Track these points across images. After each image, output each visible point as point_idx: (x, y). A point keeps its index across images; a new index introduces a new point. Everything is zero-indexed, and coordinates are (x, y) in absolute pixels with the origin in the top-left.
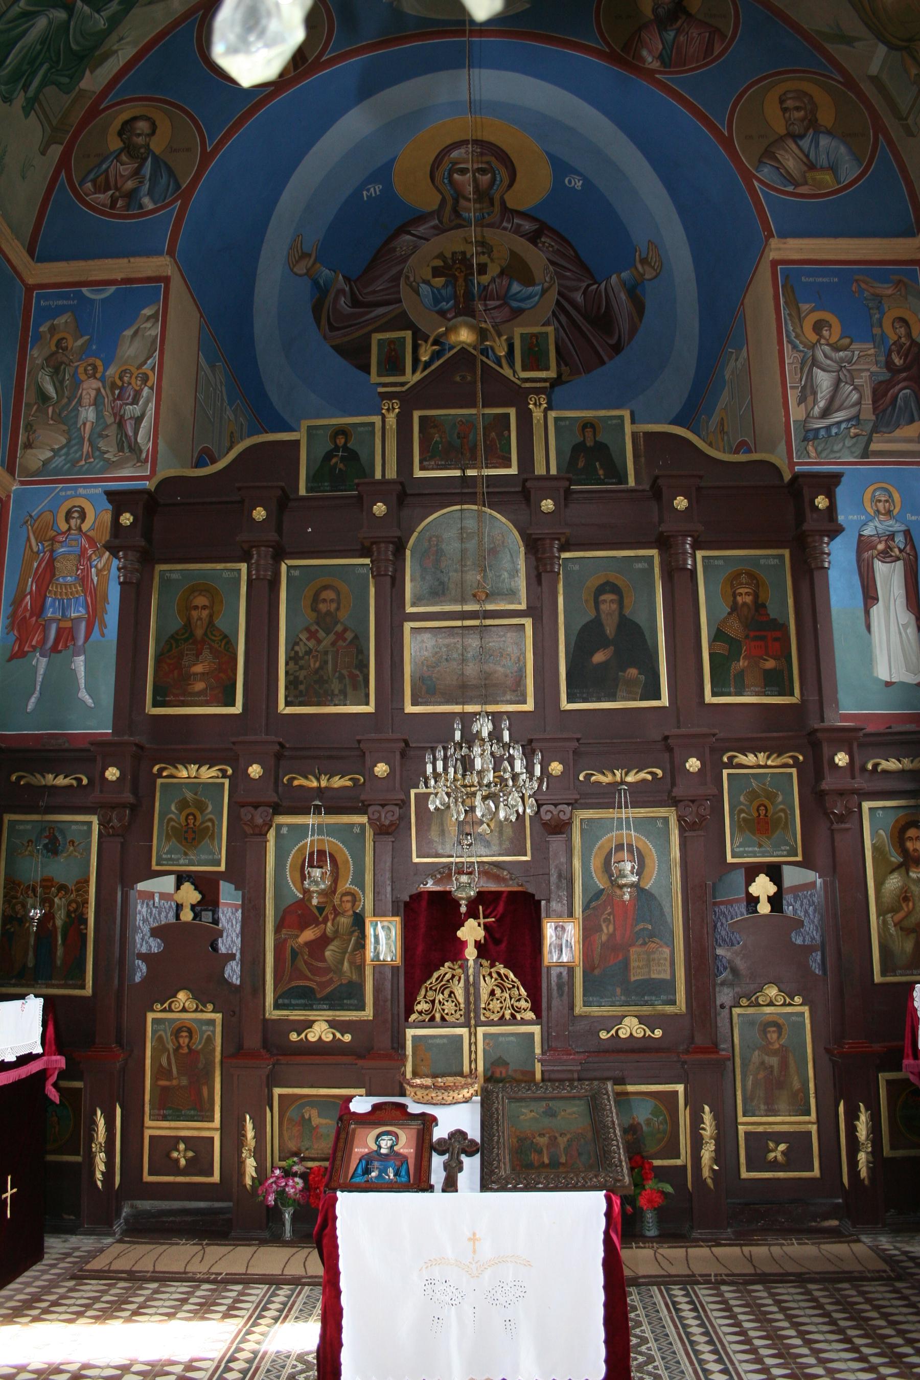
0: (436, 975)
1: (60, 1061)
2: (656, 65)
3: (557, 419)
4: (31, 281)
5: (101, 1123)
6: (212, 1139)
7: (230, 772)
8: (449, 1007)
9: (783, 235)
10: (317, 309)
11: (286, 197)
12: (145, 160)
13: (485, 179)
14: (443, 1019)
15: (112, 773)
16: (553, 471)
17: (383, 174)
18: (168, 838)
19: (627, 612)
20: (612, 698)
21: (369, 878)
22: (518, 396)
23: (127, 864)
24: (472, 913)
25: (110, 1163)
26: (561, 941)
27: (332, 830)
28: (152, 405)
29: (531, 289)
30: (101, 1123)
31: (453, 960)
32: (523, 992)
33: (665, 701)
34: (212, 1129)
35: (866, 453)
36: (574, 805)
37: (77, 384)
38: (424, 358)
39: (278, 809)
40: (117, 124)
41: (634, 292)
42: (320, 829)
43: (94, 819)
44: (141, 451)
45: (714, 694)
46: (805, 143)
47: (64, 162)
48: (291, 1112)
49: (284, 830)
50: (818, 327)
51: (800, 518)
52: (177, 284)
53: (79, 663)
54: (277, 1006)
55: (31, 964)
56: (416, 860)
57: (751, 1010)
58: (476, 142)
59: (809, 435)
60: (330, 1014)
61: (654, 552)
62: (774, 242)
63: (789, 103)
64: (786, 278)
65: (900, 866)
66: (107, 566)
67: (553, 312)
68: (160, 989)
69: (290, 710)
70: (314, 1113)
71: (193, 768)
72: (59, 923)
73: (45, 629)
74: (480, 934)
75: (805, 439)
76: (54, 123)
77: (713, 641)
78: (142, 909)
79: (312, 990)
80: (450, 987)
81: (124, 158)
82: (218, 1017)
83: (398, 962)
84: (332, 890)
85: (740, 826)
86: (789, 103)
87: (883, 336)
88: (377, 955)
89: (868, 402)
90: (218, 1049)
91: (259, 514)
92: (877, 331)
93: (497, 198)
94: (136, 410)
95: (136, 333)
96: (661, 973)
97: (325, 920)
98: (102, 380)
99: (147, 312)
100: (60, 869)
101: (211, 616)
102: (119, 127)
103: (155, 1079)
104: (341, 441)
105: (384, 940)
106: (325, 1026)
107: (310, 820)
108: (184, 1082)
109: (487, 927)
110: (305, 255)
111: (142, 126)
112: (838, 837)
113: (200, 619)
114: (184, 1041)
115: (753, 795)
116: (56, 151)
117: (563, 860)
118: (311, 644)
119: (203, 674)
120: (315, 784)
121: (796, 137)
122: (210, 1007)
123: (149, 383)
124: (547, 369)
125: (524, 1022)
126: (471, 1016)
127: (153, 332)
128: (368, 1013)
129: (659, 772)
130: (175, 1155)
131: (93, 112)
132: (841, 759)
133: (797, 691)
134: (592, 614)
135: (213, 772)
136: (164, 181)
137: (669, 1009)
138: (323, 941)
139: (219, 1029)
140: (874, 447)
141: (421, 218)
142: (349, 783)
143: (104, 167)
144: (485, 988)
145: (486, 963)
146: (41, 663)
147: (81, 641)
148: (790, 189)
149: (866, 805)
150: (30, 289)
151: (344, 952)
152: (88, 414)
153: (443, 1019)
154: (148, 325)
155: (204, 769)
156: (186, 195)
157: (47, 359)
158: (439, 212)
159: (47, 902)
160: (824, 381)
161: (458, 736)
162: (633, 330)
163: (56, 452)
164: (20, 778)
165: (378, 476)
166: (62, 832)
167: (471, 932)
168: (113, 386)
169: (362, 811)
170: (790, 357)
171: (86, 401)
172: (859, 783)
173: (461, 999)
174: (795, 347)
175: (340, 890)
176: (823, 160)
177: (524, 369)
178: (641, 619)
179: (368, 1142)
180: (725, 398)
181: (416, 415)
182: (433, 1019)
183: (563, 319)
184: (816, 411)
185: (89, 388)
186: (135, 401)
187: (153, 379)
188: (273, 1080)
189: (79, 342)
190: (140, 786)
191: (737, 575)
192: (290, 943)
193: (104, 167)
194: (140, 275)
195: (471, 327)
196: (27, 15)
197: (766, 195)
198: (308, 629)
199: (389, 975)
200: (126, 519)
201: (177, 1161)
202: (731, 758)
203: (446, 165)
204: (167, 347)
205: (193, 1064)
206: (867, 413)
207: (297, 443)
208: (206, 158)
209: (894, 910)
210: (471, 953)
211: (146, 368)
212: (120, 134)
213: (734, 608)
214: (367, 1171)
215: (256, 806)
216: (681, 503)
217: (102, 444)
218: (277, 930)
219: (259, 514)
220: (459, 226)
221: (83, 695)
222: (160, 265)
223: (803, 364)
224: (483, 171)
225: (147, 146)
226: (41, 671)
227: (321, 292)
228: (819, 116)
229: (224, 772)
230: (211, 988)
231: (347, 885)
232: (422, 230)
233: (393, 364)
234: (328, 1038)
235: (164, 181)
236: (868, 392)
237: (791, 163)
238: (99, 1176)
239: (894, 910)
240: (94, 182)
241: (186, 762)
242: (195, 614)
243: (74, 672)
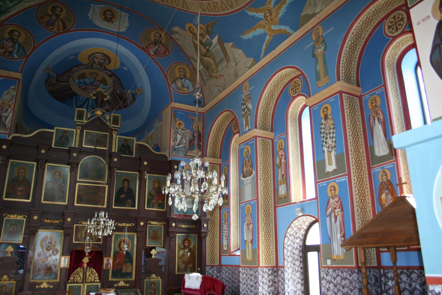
0: (76, 270)
2: (153, 54)
3: (119, 138)
7: (26, 217)
8: (79, 278)
9: (175, 102)
10: (46, 81)
11: (50, 56)
12: (16, 43)
13: (102, 61)
14: (77, 281)
16: (116, 151)
17: (76, 55)
19: (130, 186)
20: (124, 206)
22: (111, 131)
26: (108, 262)
28: (11, 114)
32: (97, 275)
33: (136, 208)
35: (186, 155)
41: (134, 97)
44: (6, 126)
45: (147, 207)
46: (183, 80)
50: (180, 124)
51: (200, 229)
57: (149, 280)
58: (102, 53)
59: (174, 149)
61: (137, 173)
62: (173, 103)
63: (181, 70)
64: (174, 111)
65: (183, 248)
69: (44, 202)
75: (173, 150)
77: (148, 195)
81: (9, 41)
85: (150, 238)
86: (181, 70)
87: (193, 129)
89: (188, 143)
92: (192, 127)
93: (104, 66)
95: (8, 92)
96: (129, 271)
99: (12, 87)
102: (9, 31)
104: (65, 134)
109: (89, 259)
110: (49, 69)
111: (16, 33)
112: (171, 242)
113: (21, 175)
115: (154, 231)
119: (21, 190)
121: (181, 79)
122: (159, 277)
123: (11, 108)
125: (97, 282)
129: (133, 224)
132: (174, 225)
133: (165, 208)
134: (122, 186)
135: (22, 217)
136: (21, 51)
137: (131, 279)
140: (188, 154)
141: (82, 65)
142: (59, 222)
143: (3, 42)
144: (88, 274)
145: (89, 268)
148: (178, 91)
149: (177, 235)
153: (77, 281)
154: (12, 91)
156: (27, 57)
158: (87, 65)
160: (179, 137)
161: (96, 216)
162: (131, 104)
167: (86, 260)
170: (173, 130)
172: (176, 230)
174: (174, 128)
176: (186, 85)
177: (113, 124)
178: (133, 188)
180: (153, 131)
181: (85, 131)
182: (74, 281)
184: (176, 144)
186: (6, 112)
187: (12, 107)
191: (155, 181)
193: (3, 42)
194: (11, 76)
195: (101, 111)
197: (173, 91)
202: (150, 222)
203: (93, 56)
206: (187, 146)
207: (53, 133)
208: (35, 48)
209: (181, 258)
211: (10, 103)
212: (9, 33)
213: (154, 188)
216: (145, 163)
220: (91, 68)
223: (175, 132)
224: (102, 60)
225: (17, 40)
227: (49, 77)
228: (187, 75)
232: (81, 67)
233: (80, 116)
234: (46, 287)
235: (21, 51)
236: (188, 141)
237: (179, 85)
239: (181, 258)
242: (20, 174)
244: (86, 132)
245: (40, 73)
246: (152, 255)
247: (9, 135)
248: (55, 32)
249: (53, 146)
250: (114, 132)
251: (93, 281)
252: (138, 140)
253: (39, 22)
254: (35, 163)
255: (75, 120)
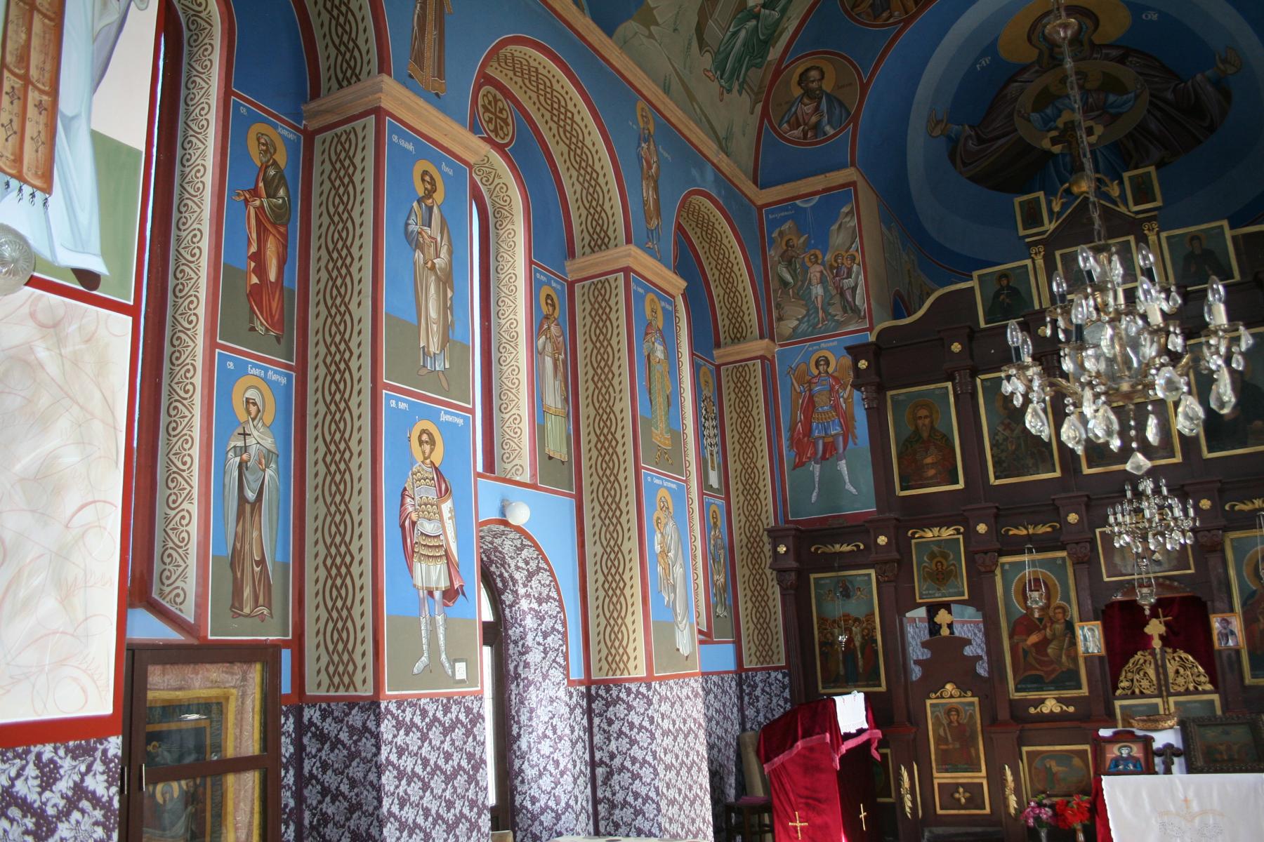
0: (1132, 661)
1: (878, 733)
3: (1168, 238)
4: (759, 203)
5: (905, 775)
6: (981, 784)
7: (962, 530)
8: (1145, 683)
10: (952, 157)
14: (1141, 692)
15: (882, 540)
18: (925, 579)
20: (1244, 445)
21: (1073, 594)
23: (898, 600)
24: (1154, 615)
25: (914, 801)
26: (1229, 629)
27: (1042, 563)
28: (861, 277)
29: (1125, 97)
30: (905, 775)
31: (1144, 649)
34: (980, 777)
36: (1226, 529)
37: (806, 270)
38: (1056, 208)
39: (1002, 553)
40: (796, 77)
41: (1220, 85)
42: (1033, 563)
43: (872, 572)
47: (765, 114)
48: (1037, 763)
49: (1007, 567)
52: (861, 185)
53: (843, 466)
54: (1017, 690)
55: (842, 673)
56: (1106, 579)
60: (1056, 693)
66: (851, 395)
67: (1149, 111)
68: (932, 682)
69: (998, 482)
70: (1053, 763)
71: (936, 530)
72: (857, 644)
73: (815, 445)
74: (1162, 629)
76: (756, 89)
78: (910, 630)
79: (1041, 677)
80: (1141, 672)
81: (806, 101)
82: (976, 699)
83: (1103, 653)
84: (1047, 606)
88: (1087, 649)
90: (979, 722)
91: (956, 347)
94: (851, 282)
95: (840, 226)
97: (1045, 628)
98: (823, 264)
99: (845, 210)
100: (853, 607)
101: (932, 422)
103: (937, 744)
105: (1090, 638)
106: (1054, 702)
107: (1026, 558)
108: (957, 746)
109: (1167, 624)
110: (938, 122)
114: (954, 718)
116: (759, 107)
117: (1220, 570)
118: (1007, 433)
120: (1025, 532)
122: (969, 693)
124: (1154, 200)
125: (1205, 692)
126: (1163, 689)
127: (852, 224)
128: (1085, 691)
130: (957, 795)
131: (778, 73)
138: (1045, 642)
139: (977, 708)
144: (1171, 668)
145: (1169, 650)
146: (816, 469)
147: (841, 450)
150: (760, 208)
151: (1061, 649)
152: (818, 290)
153: (1141, 692)
154: (847, 219)
155: (943, 529)
157: (782, 256)
159: (848, 630)
161: (1129, 494)
163: (800, 321)
164: (817, 549)
165: (1037, 307)
166: (851, 582)
167: (1155, 628)
168: (832, 267)
169: (1062, 548)
171: (814, 281)
173: (1154, 678)
175: (1052, 606)
177: (1136, 204)
179: (1114, 751)
181: (1058, 254)
182: (1133, 692)
183: (1158, 114)
185: (815, 271)
186: (849, 276)
187: (859, 258)
188: (1021, 742)
189: (802, 240)
190: (901, 545)
192: (1021, 645)
196: (735, 34)
198: (1002, 423)
199: (1097, 662)
200: (863, 364)
201: (959, 800)
204: (864, 233)
205: (963, 735)
207: (972, 289)
208: (864, 88)
210: (1157, 644)
211: (852, 250)
212: (799, 84)
214: (1117, 766)
215: (986, 553)
217: (831, 310)
218: (1011, 637)
219: (956, 347)
221: (849, 487)
222: (848, 174)
225: (820, 88)
226: (817, 474)
227: (953, 144)
229: (957, 530)
230: (968, 680)
231: (1058, 601)
232: (1026, 76)
233: (1032, 218)
234: (1057, 710)
238: (908, 810)
240: (788, 122)
241: (930, 526)
242: (920, 422)
243: (840, 473)
244: (1061, 255)
245: (919, 146)
246: (940, 626)
247: (871, 329)
248: (899, 22)
249: (982, 325)
250: (1146, 226)
251: (1191, 688)
252: (1232, 227)
253: (850, 16)
254: (949, 385)
255: (1022, 232)
